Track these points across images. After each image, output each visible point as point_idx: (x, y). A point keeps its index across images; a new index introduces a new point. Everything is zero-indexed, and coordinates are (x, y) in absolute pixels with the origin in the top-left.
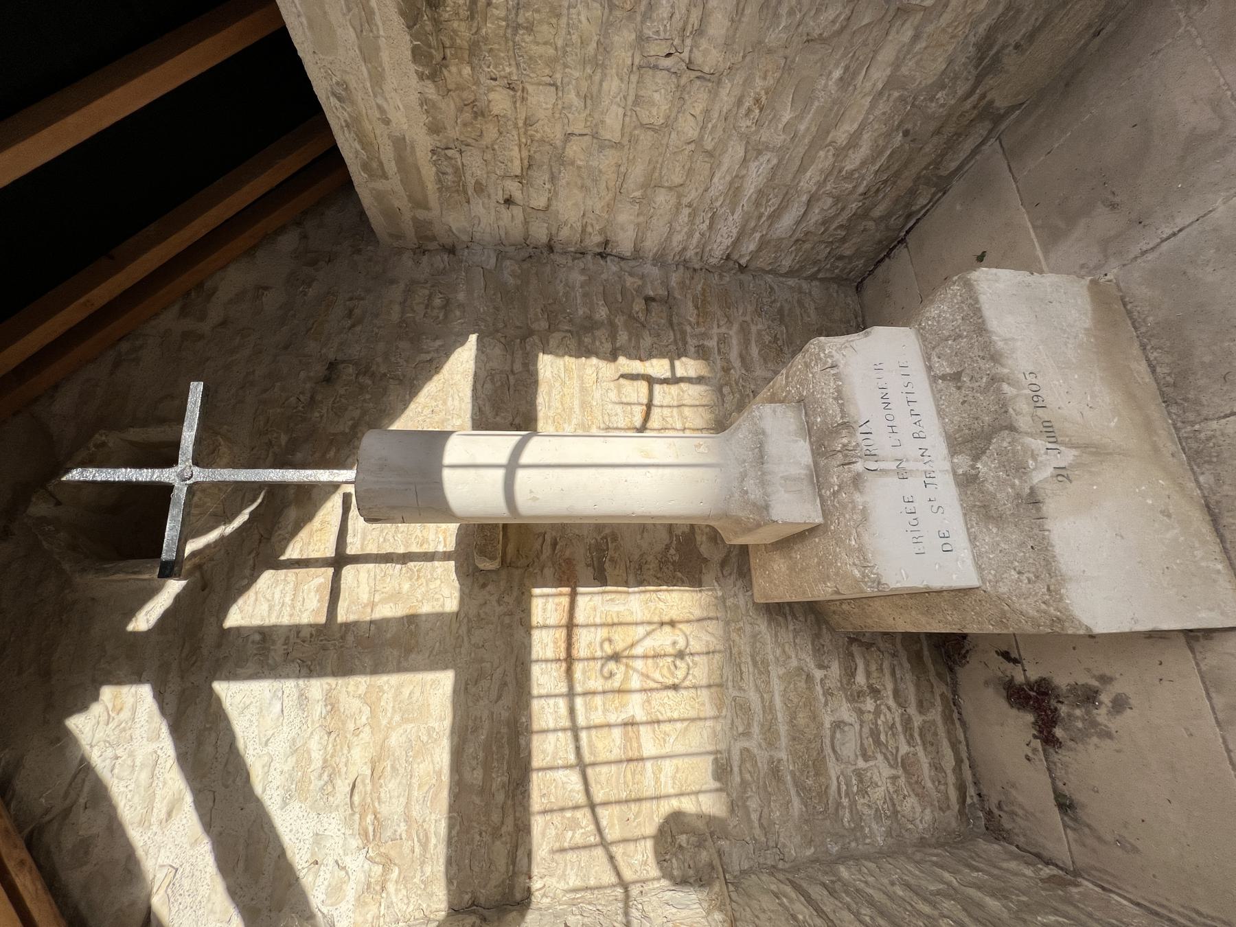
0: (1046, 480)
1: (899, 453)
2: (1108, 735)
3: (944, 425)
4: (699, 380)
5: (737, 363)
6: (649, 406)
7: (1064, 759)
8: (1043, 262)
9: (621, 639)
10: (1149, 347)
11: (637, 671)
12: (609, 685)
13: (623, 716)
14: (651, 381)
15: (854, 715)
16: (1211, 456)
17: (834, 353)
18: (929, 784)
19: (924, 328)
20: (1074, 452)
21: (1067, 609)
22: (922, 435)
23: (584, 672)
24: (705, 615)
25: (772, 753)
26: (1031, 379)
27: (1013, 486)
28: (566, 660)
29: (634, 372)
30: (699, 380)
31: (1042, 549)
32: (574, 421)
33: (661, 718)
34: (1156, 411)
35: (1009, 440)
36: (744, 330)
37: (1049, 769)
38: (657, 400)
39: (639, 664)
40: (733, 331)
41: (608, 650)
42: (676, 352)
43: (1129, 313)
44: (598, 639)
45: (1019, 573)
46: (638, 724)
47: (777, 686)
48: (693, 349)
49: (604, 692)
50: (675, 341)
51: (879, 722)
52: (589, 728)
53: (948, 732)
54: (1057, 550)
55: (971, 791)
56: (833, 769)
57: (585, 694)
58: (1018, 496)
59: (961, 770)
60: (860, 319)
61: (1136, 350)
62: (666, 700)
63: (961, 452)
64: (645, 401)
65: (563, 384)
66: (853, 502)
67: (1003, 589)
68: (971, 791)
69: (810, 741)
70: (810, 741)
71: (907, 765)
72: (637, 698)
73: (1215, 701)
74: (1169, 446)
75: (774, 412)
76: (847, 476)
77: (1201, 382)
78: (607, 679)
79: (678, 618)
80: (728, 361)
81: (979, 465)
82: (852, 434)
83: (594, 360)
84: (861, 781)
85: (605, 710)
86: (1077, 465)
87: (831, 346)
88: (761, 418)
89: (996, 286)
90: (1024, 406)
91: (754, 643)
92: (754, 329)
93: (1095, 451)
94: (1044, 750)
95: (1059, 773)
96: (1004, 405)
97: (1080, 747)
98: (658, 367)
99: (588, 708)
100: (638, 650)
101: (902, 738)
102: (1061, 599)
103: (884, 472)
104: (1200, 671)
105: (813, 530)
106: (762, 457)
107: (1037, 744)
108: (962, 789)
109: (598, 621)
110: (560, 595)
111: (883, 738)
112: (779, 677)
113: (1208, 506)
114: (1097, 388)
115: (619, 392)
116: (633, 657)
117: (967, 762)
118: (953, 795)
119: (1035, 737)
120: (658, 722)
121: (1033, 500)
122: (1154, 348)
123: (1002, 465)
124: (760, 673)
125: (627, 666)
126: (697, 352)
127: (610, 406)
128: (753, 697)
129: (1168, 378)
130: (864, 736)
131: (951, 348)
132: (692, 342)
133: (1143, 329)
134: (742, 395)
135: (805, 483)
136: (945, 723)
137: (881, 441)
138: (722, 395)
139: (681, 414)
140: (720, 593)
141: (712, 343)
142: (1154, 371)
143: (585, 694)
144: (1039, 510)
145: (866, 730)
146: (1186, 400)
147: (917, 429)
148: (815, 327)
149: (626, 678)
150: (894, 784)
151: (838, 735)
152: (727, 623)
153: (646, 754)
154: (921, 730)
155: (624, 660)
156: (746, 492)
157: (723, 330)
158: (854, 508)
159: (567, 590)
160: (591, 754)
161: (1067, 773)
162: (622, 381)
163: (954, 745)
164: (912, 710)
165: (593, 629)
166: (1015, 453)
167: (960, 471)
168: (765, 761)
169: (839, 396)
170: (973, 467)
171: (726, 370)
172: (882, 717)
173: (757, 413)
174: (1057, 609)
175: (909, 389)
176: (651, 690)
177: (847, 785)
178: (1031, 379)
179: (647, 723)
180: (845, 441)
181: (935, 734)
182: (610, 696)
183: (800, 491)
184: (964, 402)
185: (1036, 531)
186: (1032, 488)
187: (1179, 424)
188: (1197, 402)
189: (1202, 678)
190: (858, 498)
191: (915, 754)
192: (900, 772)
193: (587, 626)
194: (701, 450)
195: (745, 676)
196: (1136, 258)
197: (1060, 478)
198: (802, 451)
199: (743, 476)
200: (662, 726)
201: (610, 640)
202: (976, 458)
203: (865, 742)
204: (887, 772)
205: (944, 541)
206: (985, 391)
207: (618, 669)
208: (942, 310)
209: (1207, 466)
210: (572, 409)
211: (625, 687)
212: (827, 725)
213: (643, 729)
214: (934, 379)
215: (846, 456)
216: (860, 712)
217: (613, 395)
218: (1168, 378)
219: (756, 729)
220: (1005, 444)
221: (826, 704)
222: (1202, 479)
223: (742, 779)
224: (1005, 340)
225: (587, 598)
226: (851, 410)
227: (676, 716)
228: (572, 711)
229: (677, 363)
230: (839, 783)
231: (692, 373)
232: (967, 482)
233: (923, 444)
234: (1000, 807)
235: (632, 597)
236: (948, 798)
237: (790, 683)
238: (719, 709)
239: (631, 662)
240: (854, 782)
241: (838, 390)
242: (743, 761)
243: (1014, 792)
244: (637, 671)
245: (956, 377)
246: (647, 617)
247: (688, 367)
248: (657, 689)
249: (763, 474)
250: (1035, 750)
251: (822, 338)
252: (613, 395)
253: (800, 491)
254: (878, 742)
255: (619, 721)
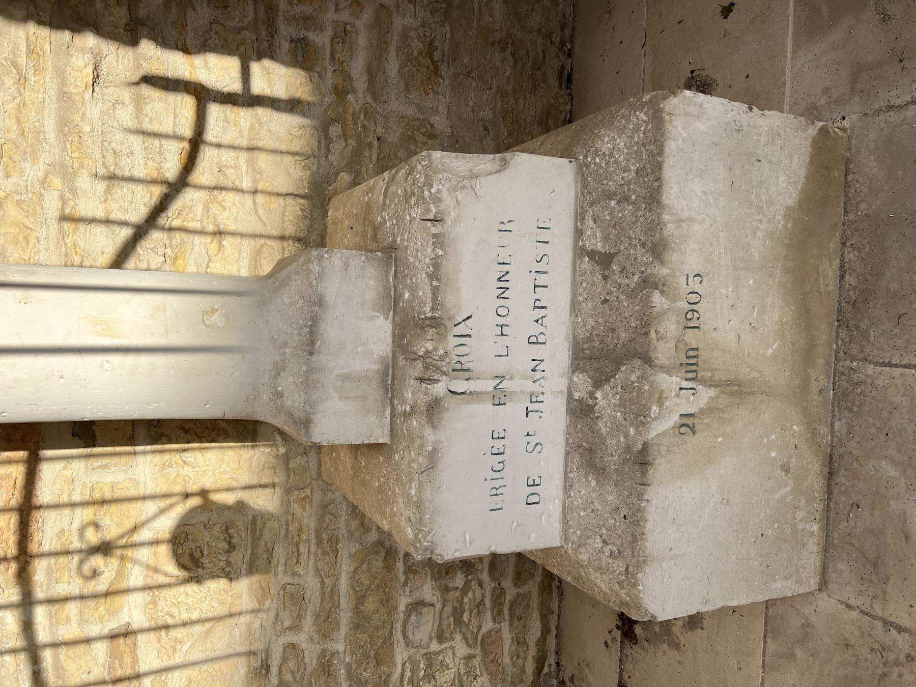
0: (664, 434)
1: (501, 366)
2: (676, 646)
3: (575, 326)
4: (291, 106)
5: (360, 83)
6: (196, 143)
7: (635, 655)
8: (789, 62)
9: (113, 524)
10: (849, 243)
11: (141, 564)
12: (91, 587)
13: (112, 625)
14: (203, 96)
15: (438, 593)
16: (853, 403)
17: (445, 194)
18: (507, 660)
19: (588, 166)
20: (712, 392)
21: (638, 597)
22: (541, 339)
23: (49, 572)
24: (255, 481)
25: (326, 646)
26: (694, 284)
27: (627, 435)
28: (16, 558)
29: (171, 74)
30: (291, 106)
31: (634, 521)
32: (45, 158)
33: (170, 621)
34: (823, 335)
35: (638, 373)
36: (381, 25)
37: (621, 660)
38: (212, 133)
39: (143, 554)
40: (363, 21)
41: (93, 537)
42: (249, 49)
43: (847, 186)
44: (76, 525)
45: (604, 542)
46: (134, 633)
47: (346, 568)
48: (286, 45)
49: (82, 597)
50: (255, 22)
51: (466, 600)
52: (55, 645)
53: (542, 604)
54: (649, 526)
55: (552, 660)
56: (401, 654)
57: (51, 601)
58: (628, 449)
59: (545, 640)
60: (568, 32)
61: (833, 244)
62: (182, 598)
63: (584, 371)
64: (188, 133)
65: (22, 79)
66: (422, 437)
67: (583, 557)
68: (552, 660)
69: (377, 628)
70: (377, 628)
71: (487, 644)
72: (138, 599)
73: (768, 646)
74: (820, 378)
75: (346, 265)
76: (423, 400)
77: (877, 312)
78: (87, 578)
79: (213, 487)
80: (348, 78)
81: (598, 395)
82: (441, 337)
83: (90, 40)
84: (430, 665)
85: (82, 621)
86: (710, 410)
87: (449, 170)
88: (320, 276)
89: (697, 123)
90: (670, 327)
91: (323, 516)
92: (398, 23)
93: (736, 389)
94: (622, 642)
95: (628, 666)
96: (648, 324)
97: (652, 649)
98: (217, 70)
99: (54, 621)
100: (145, 535)
101: (488, 615)
102: (634, 585)
103: (473, 395)
104: (766, 616)
105: (375, 448)
106: (312, 343)
107: (618, 634)
108: (540, 662)
109: (77, 498)
110: (10, 462)
111: (466, 617)
112: (351, 556)
113: (831, 457)
114: (769, 300)
115: (139, 109)
116: (134, 545)
117: (554, 632)
118: (530, 667)
119: (618, 627)
120: (167, 627)
121: (641, 460)
122: (854, 248)
123: (622, 404)
124: (325, 553)
125: (122, 558)
126: (293, 52)
127: (119, 136)
128: (311, 582)
129: (851, 293)
130: (444, 615)
131: (612, 213)
132: (285, 30)
133: (852, 217)
134: (359, 144)
135: (374, 384)
136: (541, 594)
137: (482, 350)
138: (328, 139)
139: (251, 164)
140: (282, 450)
141: (321, 39)
142: (842, 277)
143: (51, 601)
144: (644, 473)
145: (448, 609)
146: (857, 327)
147: (536, 329)
148: (498, 36)
149: (121, 574)
150: (466, 665)
151: (413, 618)
152: (288, 491)
153: (143, 668)
154: (512, 605)
155: (119, 552)
156: (281, 395)
157: (345, 16)
158: (422, 447)
159: (22, 454)
160: (58, 677)
161: (634, 668)
162: (145, 90)
163: (544, 620)
164: (507, 583)
165: (67, 511)
166: (640, 393)
167: (576, 396)
168: (315, 655)
169: (436, 272)
170: (592, 395)
171: (341, 93)
172: (470, 595)
173: (315, 267)
174: (628, 595)
175: (541, 267)
176: (160, 587)
177: (412, 671)
178: (694, 284)
179: (149, 630)
180: (429, 346)
181: (528, 606)
182: (91, 603)
183: (364, 397)
184: (605, 301)
185: (634, 499)
186: (645, 444)
187: (841, 354)
188: (865, 335)
189: (766, 622)
190: (430, 435)
191: (498, 631)
192: (478, 651)
193: (57, 506)
194: (215, 319)
195: (303, 558)
196: (880, 110)
197: (683, 430)
198: (378, 333)
199: (279, 369)
200: (174, 633)
201: (96, 526)
202: (598, 384)
203: (445, 623)
204: (462, 650)
205: (532, 490)
206: (632, 294)
207: (107, 567)
208: (613, 142)
209: (846, 412)
210: (39, 132)
211: (124, 585)
212: (402, 608)
213: (141, 638)
214: (580, 252)
215: (426, 367)
216: (446, 589)
217: (126, 115)
218: (851, 293)
219: (308, 621)
220: (633, 378)
221: (405, 584)
222: (837, 425)
223: (280, 680)
224: (680, 221)
225: (59, 466)
226: (449, 299)
227: (195, 616)
228: (27, 626)
229: (255, 68)
230: (403, 670)
231: (280, 91)
232: (581, 411)
233: (537, 352)
234: (572, 679)
235: (140, 459)
236: (523, 671)
237: (362, 562)
238: (261, 601)
239: (129, 553)
240: (422, 666)
241: (436, 264)
242: (284, 659)
243: (587, 671)
244: (141, 564)
245: (604, 260)
246: (163, 488)
247: (273, 78)
248: (169, 585)
249: (310, 370)
250: (614, 639)
251: (437, 155)
252: (126, 115)
253: (364, 397)
254: (458, 621)
255: (106, 631)
